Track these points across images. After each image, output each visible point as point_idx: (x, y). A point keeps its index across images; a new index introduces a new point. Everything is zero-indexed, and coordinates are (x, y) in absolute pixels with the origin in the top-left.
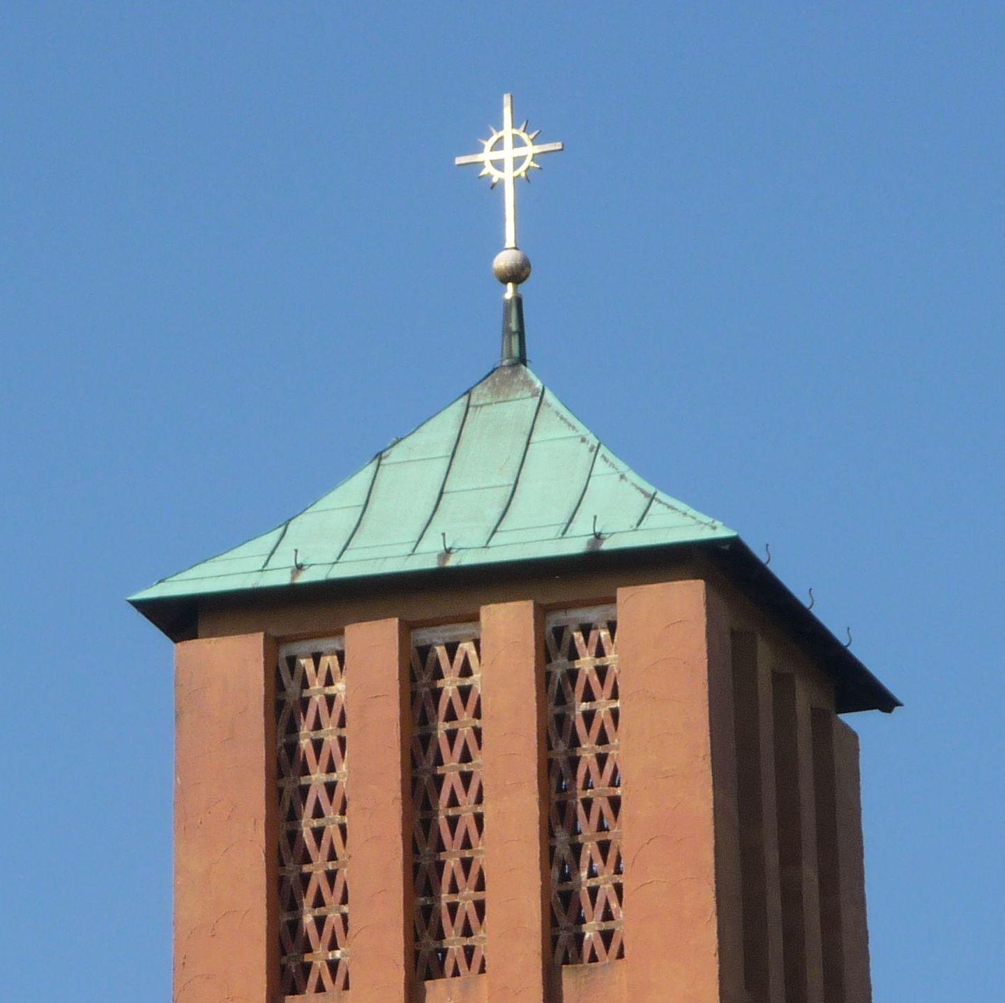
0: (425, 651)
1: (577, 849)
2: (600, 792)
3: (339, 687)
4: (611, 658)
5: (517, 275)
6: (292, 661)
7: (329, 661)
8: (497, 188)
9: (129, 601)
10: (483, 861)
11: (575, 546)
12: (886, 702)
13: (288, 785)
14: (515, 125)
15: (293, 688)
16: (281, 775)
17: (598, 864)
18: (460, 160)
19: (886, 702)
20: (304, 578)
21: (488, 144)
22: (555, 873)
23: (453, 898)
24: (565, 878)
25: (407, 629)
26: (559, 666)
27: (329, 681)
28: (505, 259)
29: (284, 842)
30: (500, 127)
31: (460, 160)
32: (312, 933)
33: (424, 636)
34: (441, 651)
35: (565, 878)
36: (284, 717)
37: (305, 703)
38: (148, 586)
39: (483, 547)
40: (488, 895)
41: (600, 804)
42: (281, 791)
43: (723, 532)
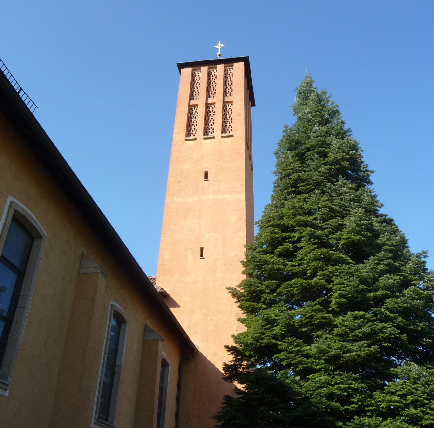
0: (210, 71)
1: (227, 88)
2: (230, 83)
6: (194, 73)
8: (218, 49)
10: (380, 240)
12: (226, 347)
13: (193, 83)
14: (220, 43)
15: (194, 75)
16: (192, 82)
17: (229, 89)
18: (214, 47)
19: (226, 347)
21: (217, 45)
22: (224, 90)
23: (228, 129)
24: (225, 90)
25: (209, 69)
27: (199, 74)
28: (218, 54)
29: (192, 87)
30: (219, 44)
31: (214, 47)
32: (195, 95)
33: (210, 70)
34: (212, 71)
35: (225, 90)
36: (193, 77)
39: (79, 272)
40: (233, 112)
41: (230, 83)
42: (192, 83)
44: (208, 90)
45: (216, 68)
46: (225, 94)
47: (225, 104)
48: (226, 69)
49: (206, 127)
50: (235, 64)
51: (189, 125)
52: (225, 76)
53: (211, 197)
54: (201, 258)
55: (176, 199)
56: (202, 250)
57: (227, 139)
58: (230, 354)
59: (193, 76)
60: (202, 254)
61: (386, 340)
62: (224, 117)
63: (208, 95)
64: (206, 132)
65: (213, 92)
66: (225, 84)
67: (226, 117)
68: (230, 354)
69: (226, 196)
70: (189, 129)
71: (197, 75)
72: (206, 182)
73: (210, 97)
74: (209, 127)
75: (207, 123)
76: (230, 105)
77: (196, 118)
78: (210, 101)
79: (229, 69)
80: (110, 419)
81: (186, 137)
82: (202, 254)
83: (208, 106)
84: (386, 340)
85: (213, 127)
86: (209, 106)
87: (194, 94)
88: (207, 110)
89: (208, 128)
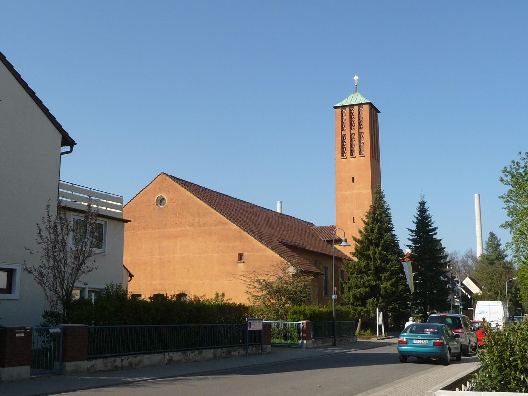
1: (360, 122)
2: (362, 118)
3: (345, 112)
4: (363, 110)
5: (357, 85)
7: (345, 110)
9: (333, 107)
11: (360, 103)
12: (380, 112)
15: (342, 112)
20: (343, 105)
26: (359, 110)
28: (356, 84)
33: (351, 108)
37: (343, 113)
38: (334, 105)
43: (370, 102)
44: (351, 126)
45: (354, 107)
46: (359, 128)
47: (360, 134)
48: (359, 108)
49: (351, 149)
50: (364, 106)
51: (343, 147)
52: (342, 152)
53: (356, 191)
54: (351, 158)
55: (340, 193)
56: (353, 178)
57: (361, 157)
58: (363, 221)
59: (342, 113)
60: (353, 181)
61: (434, 269)
62: (360, 142)
63: (351, 129)
64: (351, 155)
65: (353, 125)
66: (359, 119)
67: (361, 142)
68: (363, 221)
69: (363, 191)
70: (343, 150)
71: (344, 112)
72: (353, 183)
73: (352, 130)
74: (353, 149)
75: (351, 150)
76: (363, 134)
77: (345, 143)
78: (352, 132)
79: (361, 108)
80: (327, 294)
81: (342, 157)
82: (353, 181)
83: (351, 135)
84: (434, 269)
85: (355, 148)
86: (352, 135)
87: (344, 126)
88: (351, 137)
89: (352, 149)
